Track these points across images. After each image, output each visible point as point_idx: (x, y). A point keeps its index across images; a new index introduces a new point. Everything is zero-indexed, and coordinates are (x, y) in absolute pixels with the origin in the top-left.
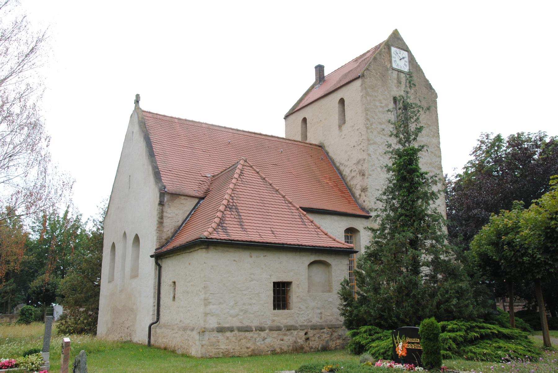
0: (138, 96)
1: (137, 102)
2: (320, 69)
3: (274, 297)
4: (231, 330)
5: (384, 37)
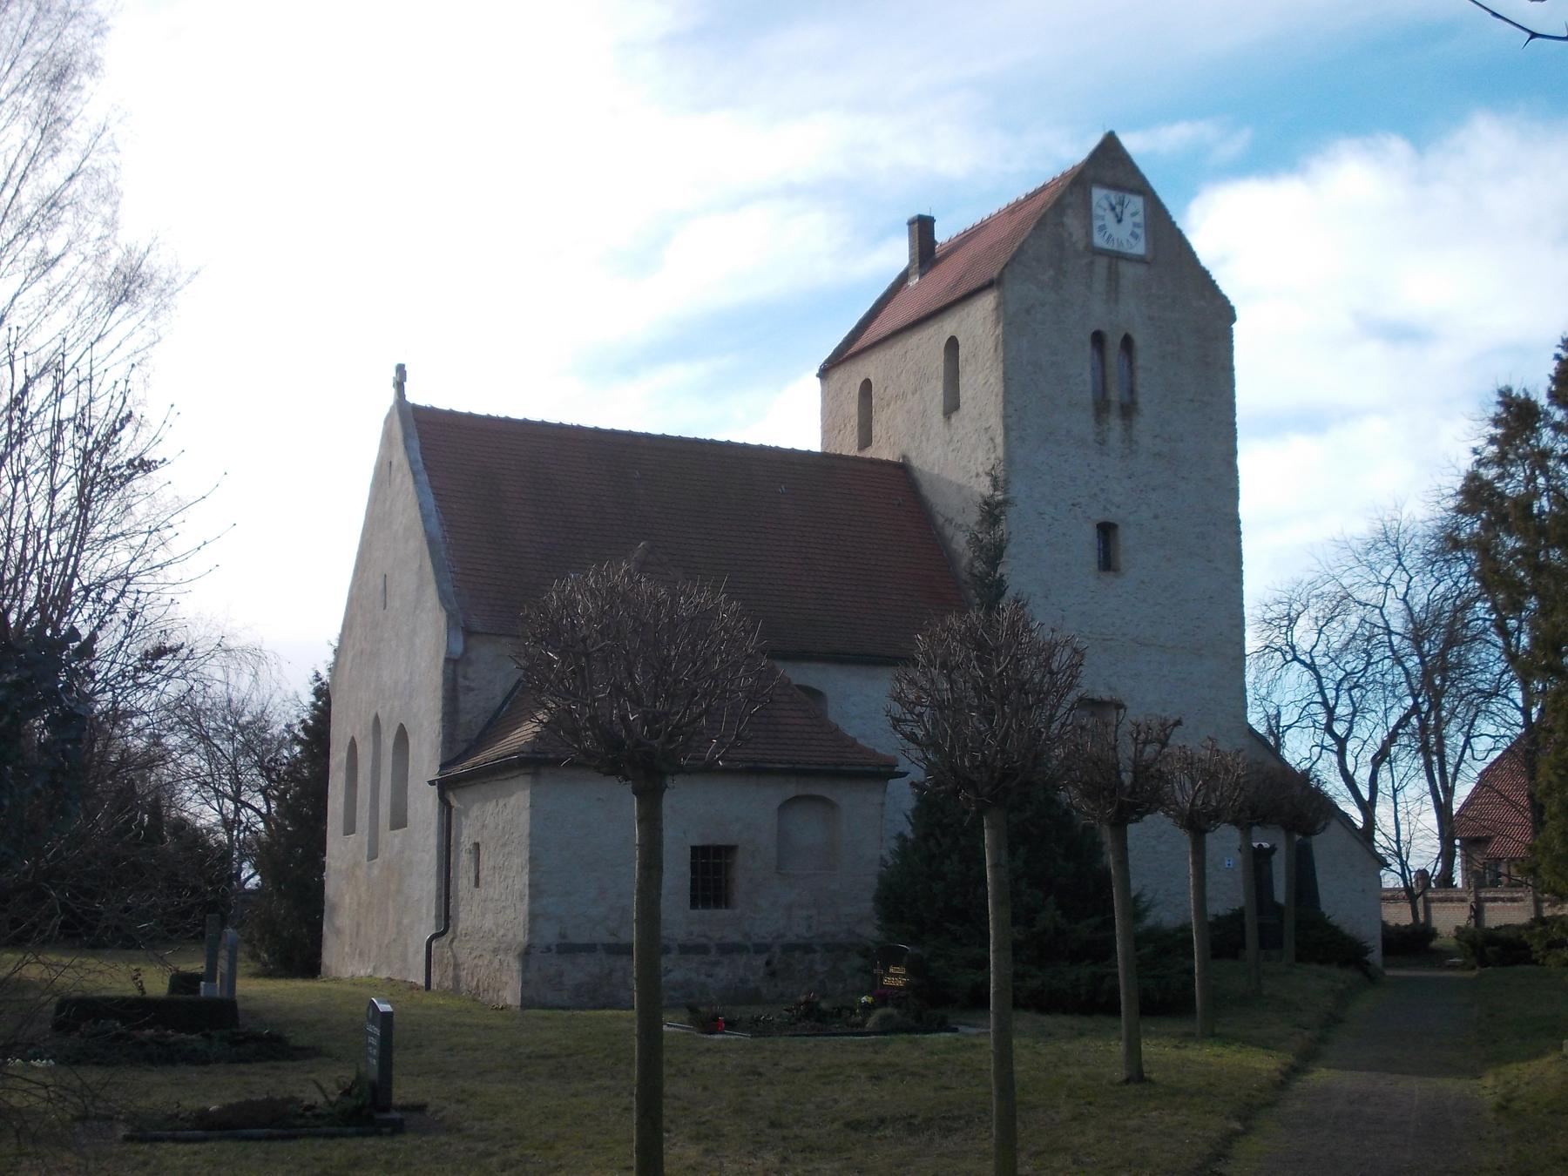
0: (401, 369)
1: (400, 385)
2: (923, 227)
3: (693, 881)
4: (590, 948)
5: (1075, 151)
